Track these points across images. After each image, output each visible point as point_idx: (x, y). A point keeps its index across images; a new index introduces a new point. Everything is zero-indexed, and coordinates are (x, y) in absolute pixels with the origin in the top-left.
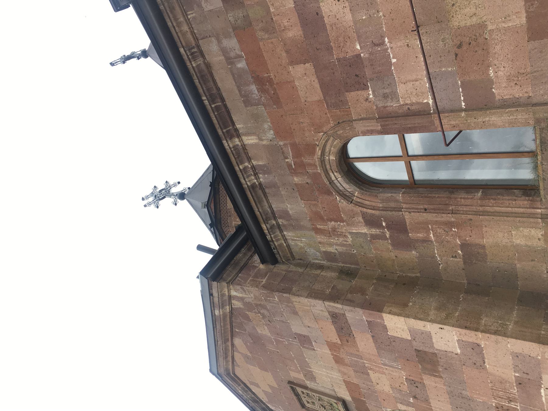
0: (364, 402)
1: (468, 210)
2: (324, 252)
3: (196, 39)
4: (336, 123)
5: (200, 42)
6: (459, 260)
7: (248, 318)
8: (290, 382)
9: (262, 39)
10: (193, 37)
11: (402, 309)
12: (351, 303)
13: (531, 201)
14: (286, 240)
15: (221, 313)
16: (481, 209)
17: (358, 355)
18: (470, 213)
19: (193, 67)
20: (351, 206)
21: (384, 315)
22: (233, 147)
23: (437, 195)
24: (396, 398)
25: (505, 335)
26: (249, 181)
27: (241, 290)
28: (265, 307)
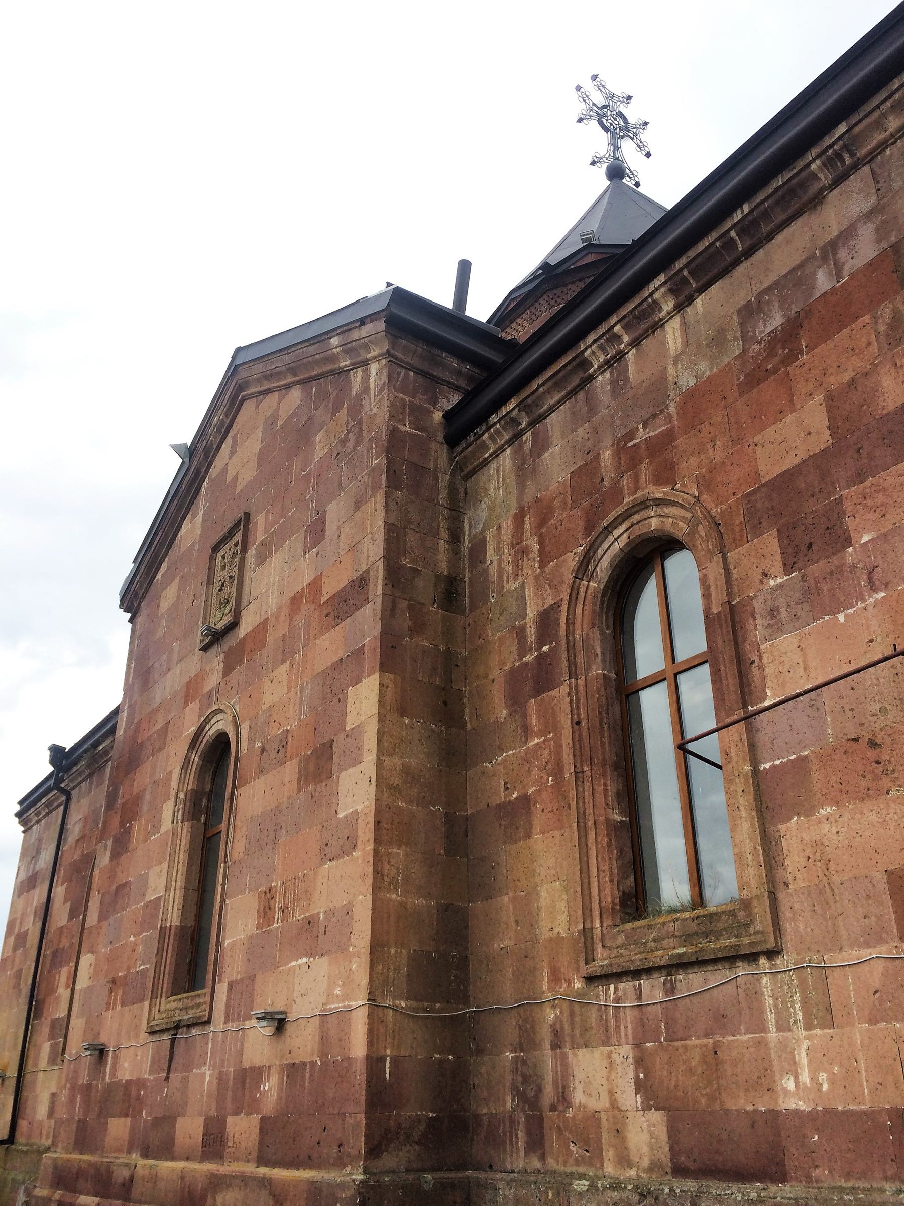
0: (241, 662)
1: (586, 800)
2: (485, 538)
3: (871, 157)
4: (717, 518)
5: (866, 169)
6: (502, 795)
7: (336, 409)
8: (247, 515)
9: (875, 318)
10: (875, 149)
11: (393, 708)
12: (390, 611)
13: (613, 908)
14: (496, 455)
15: (335, 351)
16: (590, 823)
17: (308, 639)
18: (581, 804)
19: (808, 165)
20: (569, 577)
21: (377, 676)
22: (655, 302)
23: (606, 740)
24: (256, 717)
25: (376, 889)
26: (593, 352)
27: (381, 383)
28: (358, 443)
